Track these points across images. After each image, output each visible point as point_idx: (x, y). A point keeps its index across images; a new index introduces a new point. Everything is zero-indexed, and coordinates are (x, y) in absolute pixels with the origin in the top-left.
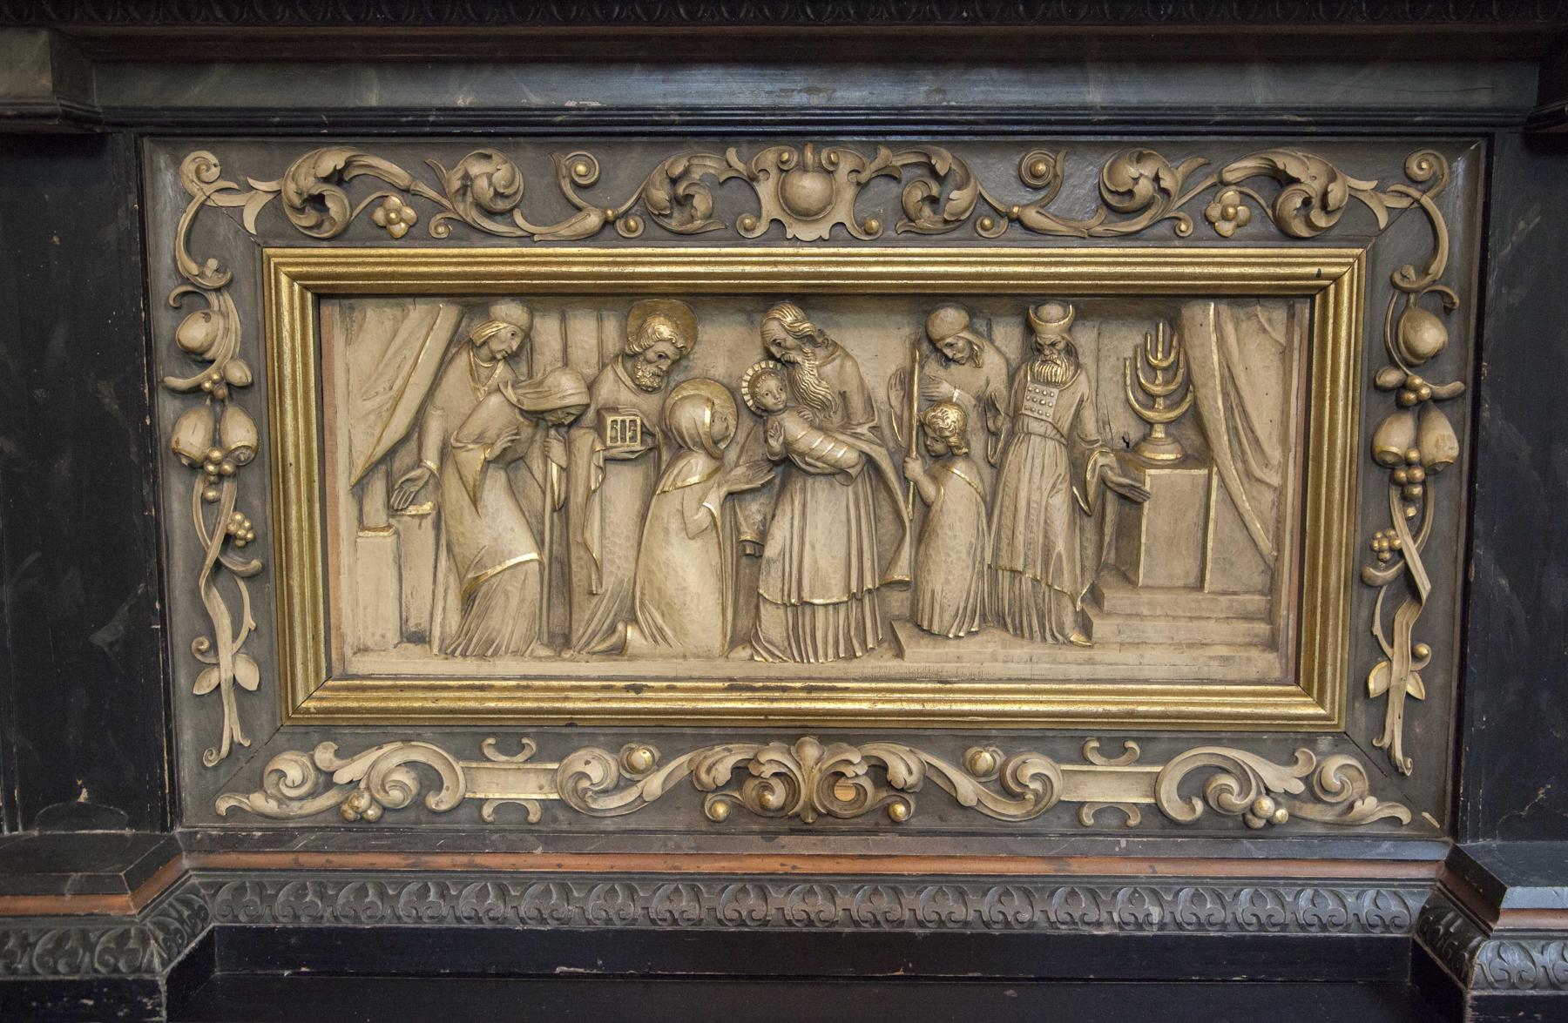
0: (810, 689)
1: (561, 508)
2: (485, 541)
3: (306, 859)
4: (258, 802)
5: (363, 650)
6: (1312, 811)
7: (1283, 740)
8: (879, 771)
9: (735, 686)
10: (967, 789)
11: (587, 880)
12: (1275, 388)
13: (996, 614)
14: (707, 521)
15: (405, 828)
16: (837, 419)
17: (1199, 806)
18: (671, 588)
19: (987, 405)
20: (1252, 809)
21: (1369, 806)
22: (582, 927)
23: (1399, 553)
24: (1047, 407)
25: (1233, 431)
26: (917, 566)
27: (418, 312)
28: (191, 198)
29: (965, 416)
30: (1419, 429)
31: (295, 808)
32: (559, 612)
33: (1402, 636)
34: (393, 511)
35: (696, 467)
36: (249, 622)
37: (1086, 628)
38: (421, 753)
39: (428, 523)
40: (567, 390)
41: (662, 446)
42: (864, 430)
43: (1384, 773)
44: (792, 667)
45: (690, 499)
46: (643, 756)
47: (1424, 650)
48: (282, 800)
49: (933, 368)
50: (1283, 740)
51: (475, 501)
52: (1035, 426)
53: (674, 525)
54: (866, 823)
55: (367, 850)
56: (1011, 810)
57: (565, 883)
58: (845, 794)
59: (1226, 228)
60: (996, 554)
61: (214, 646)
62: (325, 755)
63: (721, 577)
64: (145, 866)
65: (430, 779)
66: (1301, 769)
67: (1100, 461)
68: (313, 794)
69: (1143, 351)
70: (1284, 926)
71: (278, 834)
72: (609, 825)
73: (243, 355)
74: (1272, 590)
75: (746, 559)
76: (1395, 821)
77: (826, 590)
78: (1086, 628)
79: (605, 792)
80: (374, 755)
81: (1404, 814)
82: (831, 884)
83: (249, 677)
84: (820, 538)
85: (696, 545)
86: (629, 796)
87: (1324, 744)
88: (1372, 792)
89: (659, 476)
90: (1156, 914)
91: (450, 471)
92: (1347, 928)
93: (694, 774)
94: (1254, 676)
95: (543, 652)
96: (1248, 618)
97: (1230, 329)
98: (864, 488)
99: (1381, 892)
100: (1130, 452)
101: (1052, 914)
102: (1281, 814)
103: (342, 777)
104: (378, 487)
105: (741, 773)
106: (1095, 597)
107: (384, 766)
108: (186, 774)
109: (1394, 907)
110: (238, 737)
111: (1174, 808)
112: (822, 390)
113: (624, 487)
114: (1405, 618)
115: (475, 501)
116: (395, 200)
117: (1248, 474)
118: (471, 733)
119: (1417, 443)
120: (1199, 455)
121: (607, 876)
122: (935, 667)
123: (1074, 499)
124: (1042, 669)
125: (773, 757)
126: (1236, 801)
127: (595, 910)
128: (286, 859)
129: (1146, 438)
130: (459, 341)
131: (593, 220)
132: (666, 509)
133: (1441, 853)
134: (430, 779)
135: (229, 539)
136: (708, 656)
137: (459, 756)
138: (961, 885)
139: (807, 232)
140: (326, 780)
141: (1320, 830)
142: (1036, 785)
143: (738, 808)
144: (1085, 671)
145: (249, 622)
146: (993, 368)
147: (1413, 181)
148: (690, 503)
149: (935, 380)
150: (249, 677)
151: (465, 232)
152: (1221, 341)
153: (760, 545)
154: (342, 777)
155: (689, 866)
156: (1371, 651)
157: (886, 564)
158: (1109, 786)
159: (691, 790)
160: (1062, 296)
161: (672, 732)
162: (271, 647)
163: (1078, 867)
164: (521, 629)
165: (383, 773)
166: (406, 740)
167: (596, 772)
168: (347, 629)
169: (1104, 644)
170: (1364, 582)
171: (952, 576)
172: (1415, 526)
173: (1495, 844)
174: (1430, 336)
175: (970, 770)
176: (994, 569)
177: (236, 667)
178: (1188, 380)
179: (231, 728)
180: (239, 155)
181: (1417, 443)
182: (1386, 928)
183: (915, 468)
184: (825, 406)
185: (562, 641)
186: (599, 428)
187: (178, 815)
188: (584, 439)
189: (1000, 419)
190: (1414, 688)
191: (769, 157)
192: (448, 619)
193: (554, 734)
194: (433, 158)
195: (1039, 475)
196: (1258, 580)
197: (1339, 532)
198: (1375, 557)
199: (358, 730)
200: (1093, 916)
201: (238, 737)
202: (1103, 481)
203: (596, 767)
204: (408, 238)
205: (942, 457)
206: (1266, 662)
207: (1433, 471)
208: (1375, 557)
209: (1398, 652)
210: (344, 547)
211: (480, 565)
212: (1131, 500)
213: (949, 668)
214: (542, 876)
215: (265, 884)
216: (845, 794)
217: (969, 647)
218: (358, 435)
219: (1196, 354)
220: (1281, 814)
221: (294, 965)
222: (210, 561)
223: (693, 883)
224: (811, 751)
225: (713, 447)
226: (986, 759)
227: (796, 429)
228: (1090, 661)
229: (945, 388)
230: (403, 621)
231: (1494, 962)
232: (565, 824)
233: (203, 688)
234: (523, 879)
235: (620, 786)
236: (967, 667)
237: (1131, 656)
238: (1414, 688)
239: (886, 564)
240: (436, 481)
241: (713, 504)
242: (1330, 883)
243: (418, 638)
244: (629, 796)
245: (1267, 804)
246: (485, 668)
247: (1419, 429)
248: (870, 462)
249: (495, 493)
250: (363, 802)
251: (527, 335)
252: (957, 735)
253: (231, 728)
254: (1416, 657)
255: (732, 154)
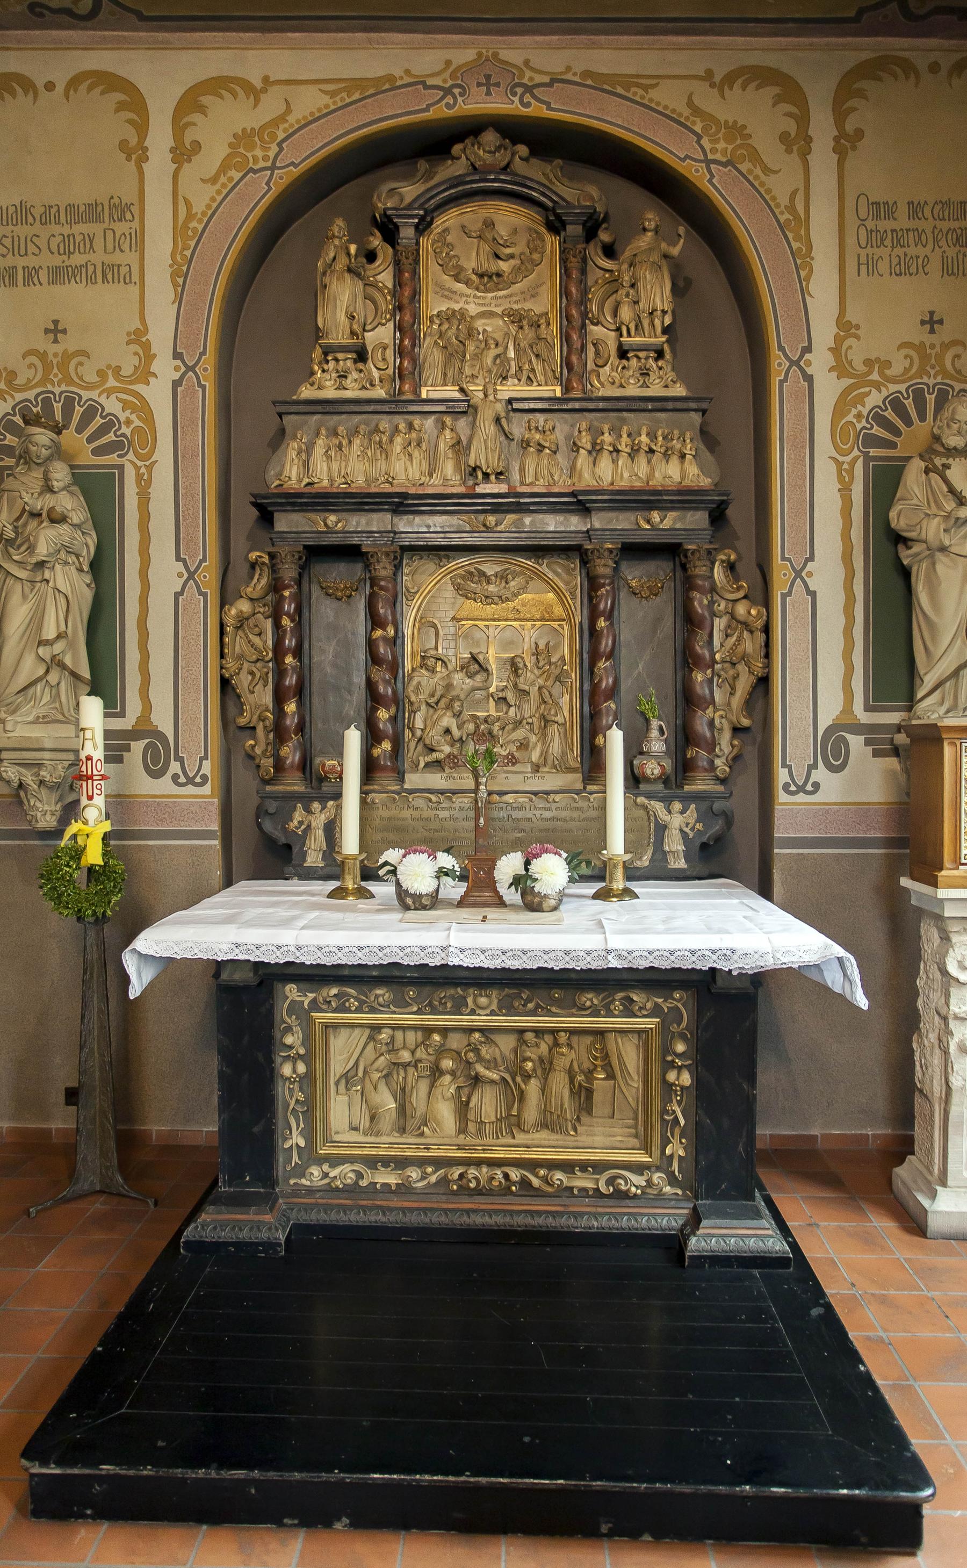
0: (484, 1150)
1: (403, 1089)
2: (378, 1101)
3: (319, 1201)
4: (304, 1181)
5: (337, 1133)
6: (649, 1191)
7: (639, 1169)
8: (506, 1176)
9: (460, 1148)
10: (536, 1182)
11: (411, 1210)
12: (635, 1057)
13: (548, 1123)
14: (450, 1095)
15: (353, 1190)
16: (493, 1065)
17: (611, 1189)
18: (439, 1117)
19: (541, 1060)
20: (628, 1190)
21: (668, 1189)
22: (410, 1226)
23: (674, 1112)
24: (562, 1063)
25: (621, 1070)
26: (519, 1110)
27: (357, 1031)
28: (288, 998)
29: (534, 1065)
30: (679, 1074)
31: (315, 1184)
32: (402, 1121)
33: (677, 1136)
34: (347, 1089)
35: (447, 1078)
36: (302, 1125)
37: (575, 1130)
38: (356, 1167)
39: (359, 1093)
40: (406, 1056)
41: (436, 1072)
42: (501, 1068)
43: (672, 1180)
44: (478, 1141)
45: (445, 1089)
46: (429, 1170)
47: (683, 1141)
48: (311, 1181)
49: (524, 1047)
50: (639, 1169)
51: (375, 1089)
52: (557, 1068)
53: (440, 1097)
54: (503, 1192)
55: (341, 1199)
56: (550, 1189)
57: (404, 1210)
58: (495, 1183)
59: (616, 1013)
60: (545, 1106)
61: (291, 1133)
62: (326, 1167)
63: (455, 1113)
64: (268, 1200)
65: (360, 1176)
66: (645, 1178)
67: (580, 1078)
68: (321, 1179)
69: (593, 1043)
70: (637, 1229)
71: (311, 1191)
72: (419, 1191)
73: (303, 1044)
74: (636, 1119)
75: (463, 1109)
76: (677, 1194)
77: (489, 1117)
78: (575, 1130)
79: (418, 1181)
80: (342, 1167)
81: (680, 1192)
82: (490, 1213)
83: (302, 1143)
84: (487, 1103)
85: (447, 1103)
86: (425, 1182)
87: (653, 1169)
88: (669, 1185)
89: (435, 1081)
90: (596, 1224)
91: (367, 1078)
92: (657, 1230)
93: (446, 1176)
94: (630, 1146)
95: (396, 1134)
96: (629, 1127)
97: (619, 1040)
98: (502, 1086)
99: (667, 1219)
100: (589, 1074)
101: (565, 1223)
102: (639, 1192)
103: (331, 1175)
104: (343, 1082)
105: (461, 1176)
106: (578, 1120)
107: (345, 1171)
108: (280, 1173)
109: (674, 1223)
110: (297, 1161)
111: (603, 1188)
112: (488, 1057)
113: (423, 1086)
114: (677, 1131)
115: (375, 1089)
116: (352, 1000)
117: (628, 1084)
118: (373, 1162)
119: (678, 1079)
120: (611, 1076)
121: (418, 1209)
122: (525, 1142)
123: (571, 1089)
124: (560, 1143)
125: (472, 1172)
126: (623, 1188)
127: (415, 1219)
128: (313, 1201)
129: (595, 1069)
130: (371, 1038)
131: (415, 1009)
132: (437, 1092)
133: (692, 1205)
134: (360, 1176)
135: (297, 1101)
136: (451, 1137)
137: (369, 1168)
138: (531, 1213)
139: (482, 1012)
140: (326, 1175)
141: (652, 1197)
142: (558, 1182)
143: (460, 1187)
144: (575, 1144)
145: (302, 1125)
146: (544, 1048)
147: (675, 999)
148: (445, 1089)
149: (524, 1051)
150: (302, 1143)
151: (373, 1010)
152: (617, 1043)
153: (468, 1102)
154: (331, 1175)
155: (445, 1206)
156: (665, 1142)
157: (509, 1109)
158: (582, 1182)
159: (444, 1181)
160: (565, 1030)
161: (439, 1163)
162: (309, 1134)
163: (571, 1209)
164: (390, 1127)
165: (344, 1174)
166: (352, 1163)
167: (414, 1175)
168: (332, 1126)
169: (581, 1134)
170: (663, 1120)
171: (531, 1113)
172: (679, 1103)
173: (708, 1202)
174: (680, 1048)
175: (537, 1176)
176: (545, 1110)
177: (297, 1139)
178: (607, 1053)
179: (295, 1158)
180: (302, 986)
181: (678, 1079)
182: (670, 1230)
183: (518, 1079)
184: (489, 1061)
185: (403, 1130)
186: (416, 1066)
187: (278, 1184)
188: (411, 1070)
189: (546, 1066)
190: (681, 1152)
191: (471, 990)
192: (365, 1123)
193: (401, 1163)
194: (365, 989)
195: (559, 1084)
196: (631, 1115)
197: (656, 1105)
198: (667, 1112)
199: (336, 1161)
200: (576, 1225)
201: (297, 1161)
202: (580, 1085)
203: (414, 1173)
204: (356, 1011)
205: (527, 1077)
206: (635, 1142)
207: (682, 1088)
208: (667, 1112)
209: (676, 1140)
210: (332, 1101)
211: (377, 1108)
212: (590, 1092)
213: (529, 1142)
214: (396, 1209)
215: (308, 1208)
216: (495, 1183)
217: (537, 1136)
218: (338, 1066)
219: (609, 1047)
220: (639, 1192)
221: (317, 1236)
222: (291, 1107)
223: (445, 1211)
224: (484, 1169)
225: (453, 1073)
226: (542, 1172)
227: (480, 1069)
228: (577, 1141)
229: (529, 1054)
230: (350, 1124)
231: (695, 1244)
232: (404, 1189)
233: (287, 1146)
234: (391, 1209)
235: (423, 1178)
236: (536, 1142)
237: (590, 1138)
238: (681, 1152)
239: (509, 1109)
240: (363, 1080)
241: (452, 1090)
242: (654, 1215)
243: (356, 1129)
244: (425, 1182)
245: (633, 1189)
246: (378, 1140)
247: (679, 1074)
248: (503, 1079)
249: (382, 1087)
250: (338, 1183)
251: (392, 1038)
252: (533, 1165)
253: (295, 1158)
254: (681, 1143)
255: (459, 990)
